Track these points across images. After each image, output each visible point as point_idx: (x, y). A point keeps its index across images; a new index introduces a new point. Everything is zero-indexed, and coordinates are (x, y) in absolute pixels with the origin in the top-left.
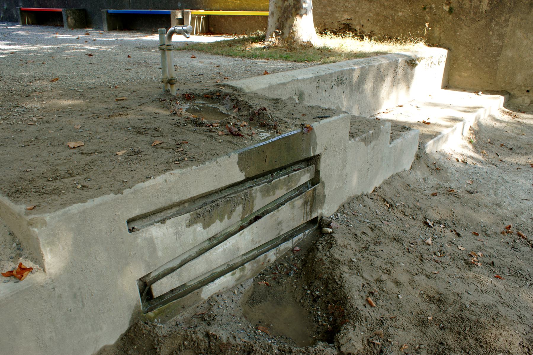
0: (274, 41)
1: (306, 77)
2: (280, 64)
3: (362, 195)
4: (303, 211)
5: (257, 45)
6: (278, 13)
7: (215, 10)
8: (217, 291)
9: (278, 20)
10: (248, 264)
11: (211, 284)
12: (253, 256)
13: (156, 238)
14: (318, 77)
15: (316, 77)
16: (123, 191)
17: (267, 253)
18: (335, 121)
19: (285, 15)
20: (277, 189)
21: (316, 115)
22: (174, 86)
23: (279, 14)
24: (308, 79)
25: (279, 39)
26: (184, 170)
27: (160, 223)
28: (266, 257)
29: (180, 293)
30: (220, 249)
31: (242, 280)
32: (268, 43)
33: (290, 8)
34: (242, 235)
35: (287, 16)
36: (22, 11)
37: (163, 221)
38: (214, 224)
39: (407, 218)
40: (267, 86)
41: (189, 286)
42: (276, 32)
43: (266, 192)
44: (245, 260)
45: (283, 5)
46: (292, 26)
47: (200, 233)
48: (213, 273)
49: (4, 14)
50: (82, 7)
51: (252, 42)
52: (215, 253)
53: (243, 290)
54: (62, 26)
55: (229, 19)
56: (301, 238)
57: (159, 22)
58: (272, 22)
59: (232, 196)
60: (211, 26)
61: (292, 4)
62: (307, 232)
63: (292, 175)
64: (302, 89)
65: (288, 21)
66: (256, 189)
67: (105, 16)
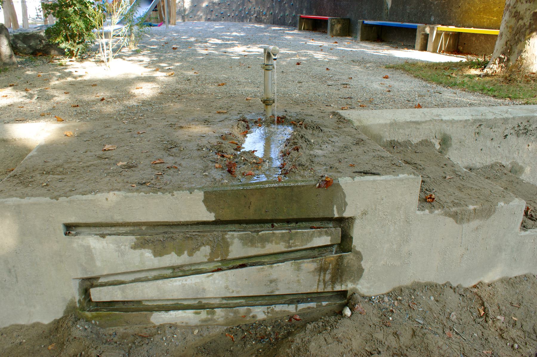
0: (495, 69)
1: (456, 118)
2: (472, 98)
3: (444, 285)
4: (317, 278)
5: (474, 72)
6: (508, 34)
7: (467, 27)
8: (173, 323)
9: (506, 43)
10: (220, 309)
11: (163, 312)
12: (229, 303)
13: (94, 248)
14: (480, 120)
15: (475, 121)
16: (59, 198)
17: (251, 308)
18: (386, 181)
19: (516, 38)
20: (268, 242)
21: (354, 171)
22: (269, 107)
23: (508, 35)
24: (461, 121)
25: (502, 67)
26: (130, 194)
27: (98, 236)
28: (249, 311)
29: (133, 308)
30: (178, 282)
31: (209, 323)
32: (488, 70)
33: (523, 30)
34: (211, 278)
35: (518, 38)
36: (301, 18)
37: (103, 236)
38: (169, 255)
39: (501, 343)
40: (388, 122)
41: (144, 305)
42: (500, 58)
43: (248, 242)
44: (223, 304)
45: (516, 24)
46: (521, 51)
47: (147, 258)
48: (178, 304)
49: (292, 20)
50: (348, 16)
51: (470, 68)
52: (169, 284)
53: (205, 333)
54: (325, 32)
55: (481, 37)
56: (313, 308)
57: (405, 37)
58: (499, 45)
59: (194, 234)
60: (458, 43)
61: (528, 24)
62: (324, 303)
63: (297, 233)
64: (448, 133)
65: (519, 46)
66: (233, 235)
67: (359, 27)
